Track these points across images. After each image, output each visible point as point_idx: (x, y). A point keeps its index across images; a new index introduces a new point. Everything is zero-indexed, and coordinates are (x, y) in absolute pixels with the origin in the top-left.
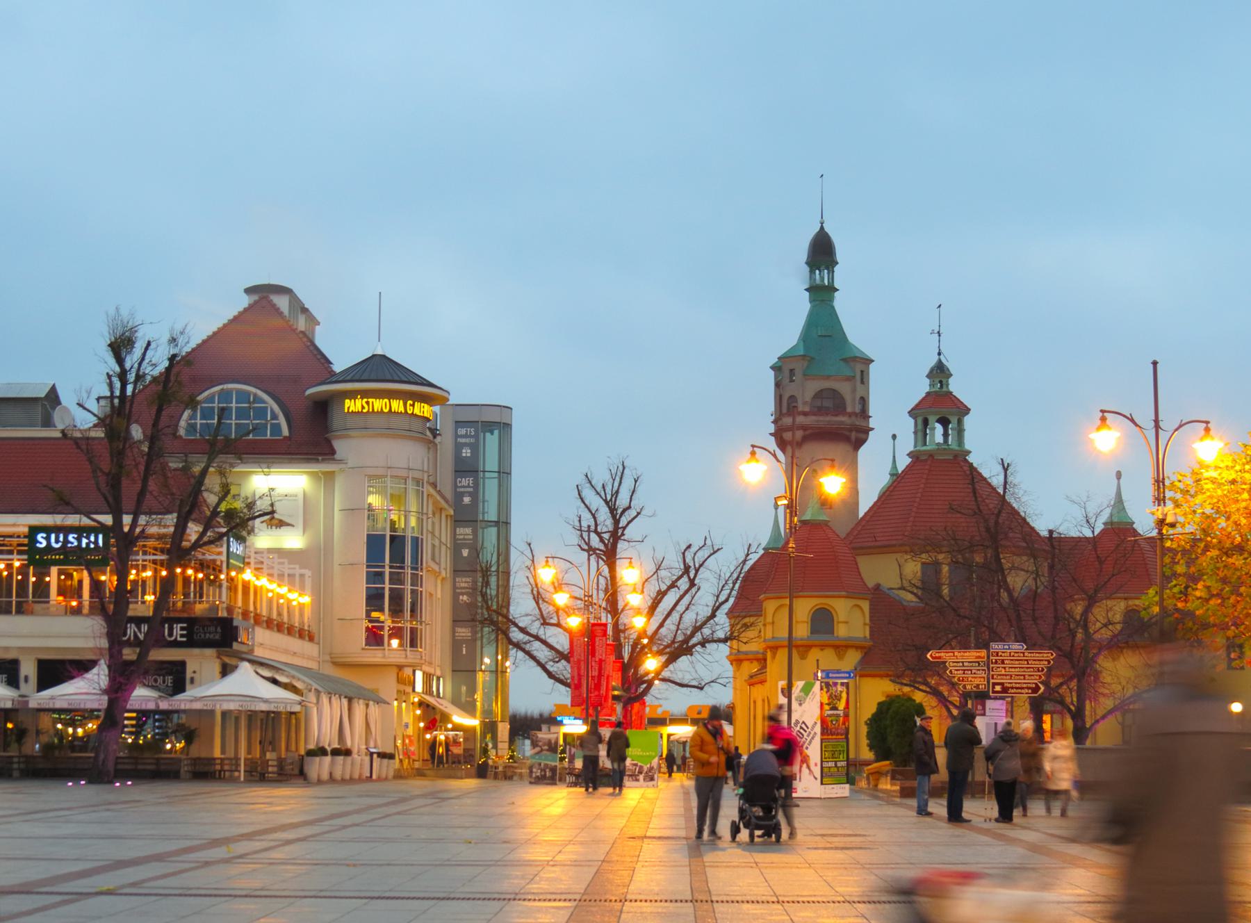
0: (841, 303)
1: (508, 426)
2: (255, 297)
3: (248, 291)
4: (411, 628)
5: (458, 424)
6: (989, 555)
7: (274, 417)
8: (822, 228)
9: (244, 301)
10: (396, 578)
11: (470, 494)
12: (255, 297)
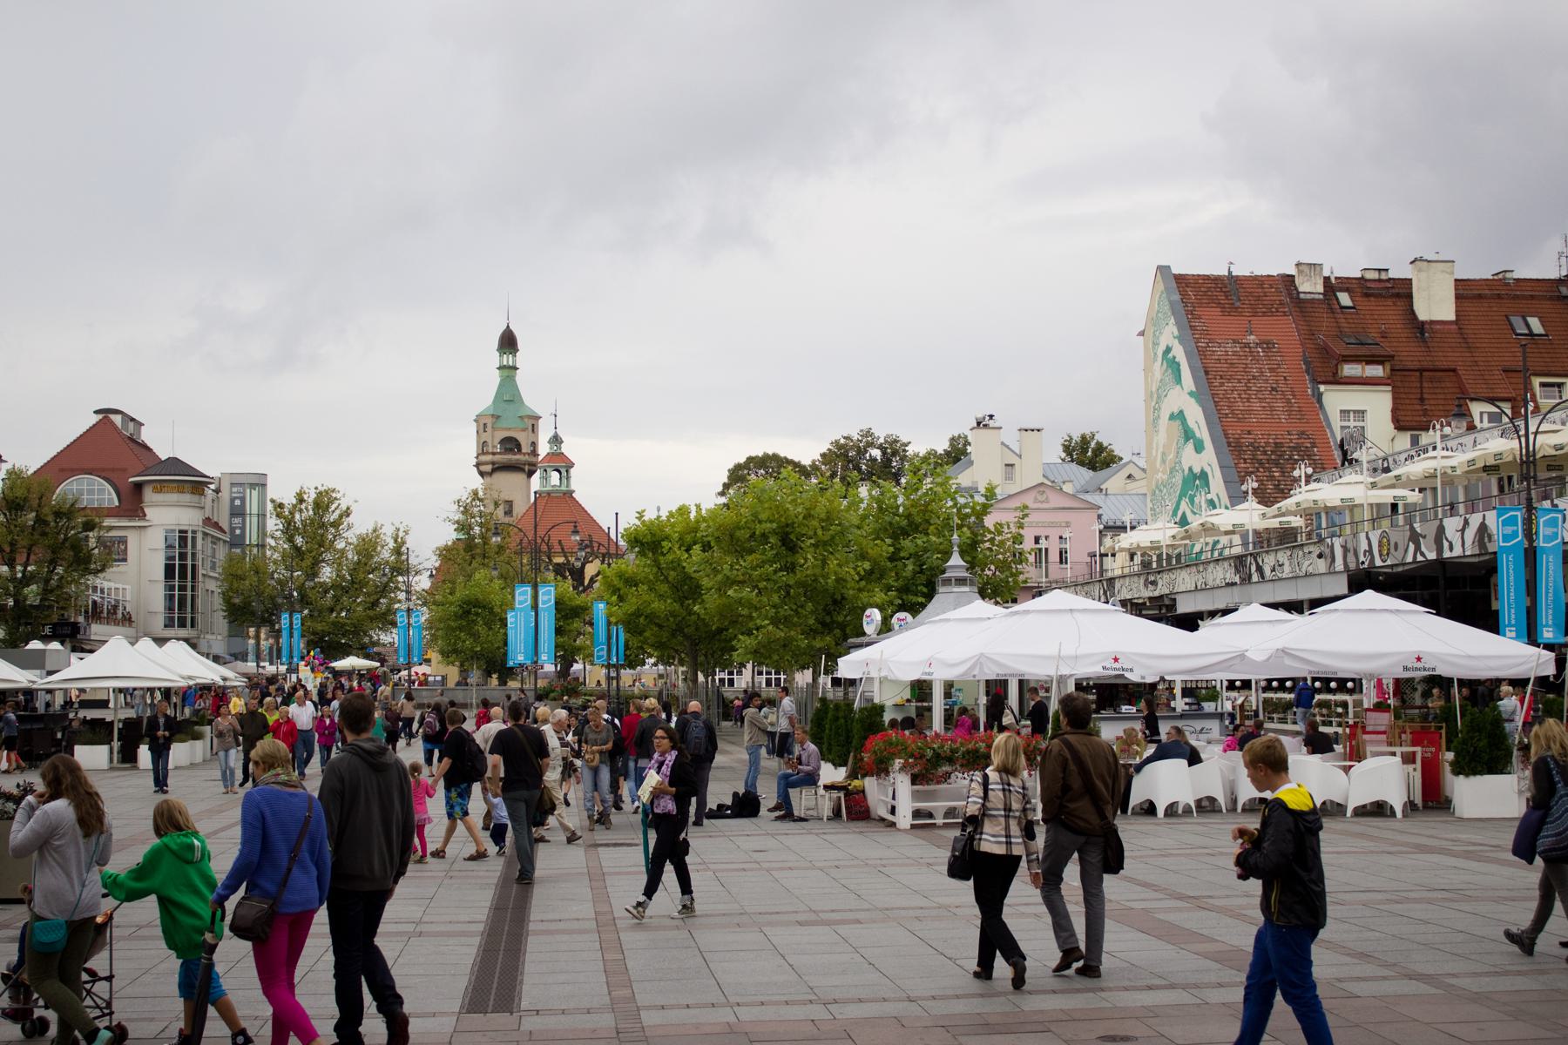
0: (520, 377)
1: (264, 485)
2: (100, 416)
3: (96, 412)
4: (917, 701)
5: (233, 485)
6: (525, 561)
7: (110, 494)
8: (508, 326)
9: (96, 418)
10: (182, 588)
11: (240, 528)
12: (100, 416)
